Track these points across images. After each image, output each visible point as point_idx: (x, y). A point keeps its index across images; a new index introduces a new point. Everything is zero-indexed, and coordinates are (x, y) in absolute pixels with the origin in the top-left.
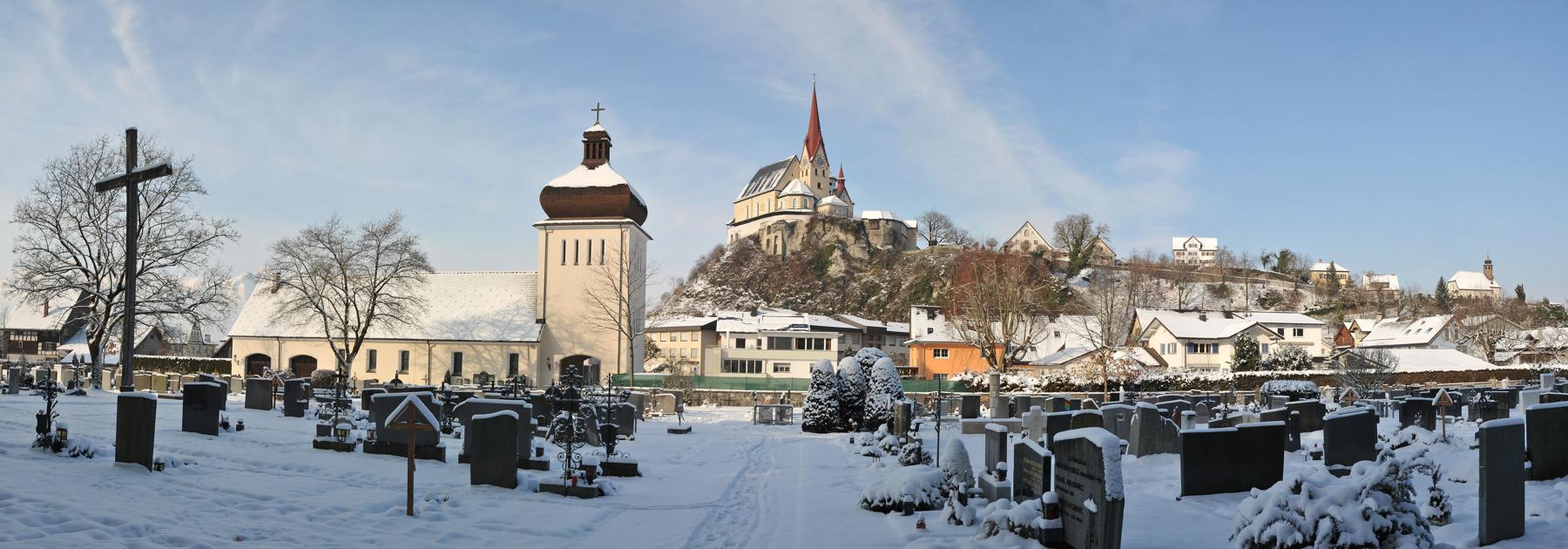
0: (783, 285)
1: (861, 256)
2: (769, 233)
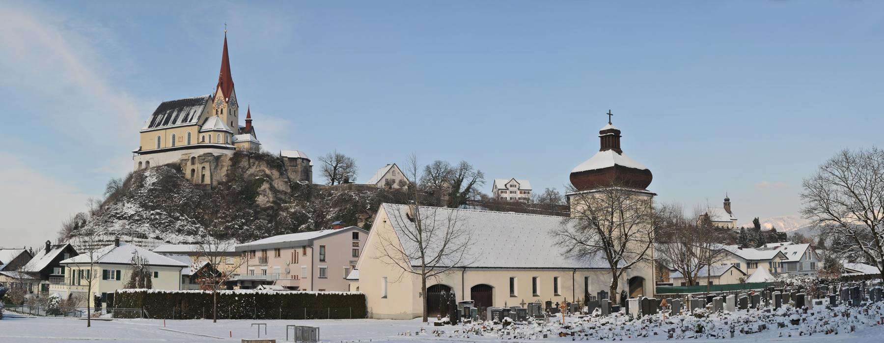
0: (217, 212)
1: (284, 189)
2: (193, 163)
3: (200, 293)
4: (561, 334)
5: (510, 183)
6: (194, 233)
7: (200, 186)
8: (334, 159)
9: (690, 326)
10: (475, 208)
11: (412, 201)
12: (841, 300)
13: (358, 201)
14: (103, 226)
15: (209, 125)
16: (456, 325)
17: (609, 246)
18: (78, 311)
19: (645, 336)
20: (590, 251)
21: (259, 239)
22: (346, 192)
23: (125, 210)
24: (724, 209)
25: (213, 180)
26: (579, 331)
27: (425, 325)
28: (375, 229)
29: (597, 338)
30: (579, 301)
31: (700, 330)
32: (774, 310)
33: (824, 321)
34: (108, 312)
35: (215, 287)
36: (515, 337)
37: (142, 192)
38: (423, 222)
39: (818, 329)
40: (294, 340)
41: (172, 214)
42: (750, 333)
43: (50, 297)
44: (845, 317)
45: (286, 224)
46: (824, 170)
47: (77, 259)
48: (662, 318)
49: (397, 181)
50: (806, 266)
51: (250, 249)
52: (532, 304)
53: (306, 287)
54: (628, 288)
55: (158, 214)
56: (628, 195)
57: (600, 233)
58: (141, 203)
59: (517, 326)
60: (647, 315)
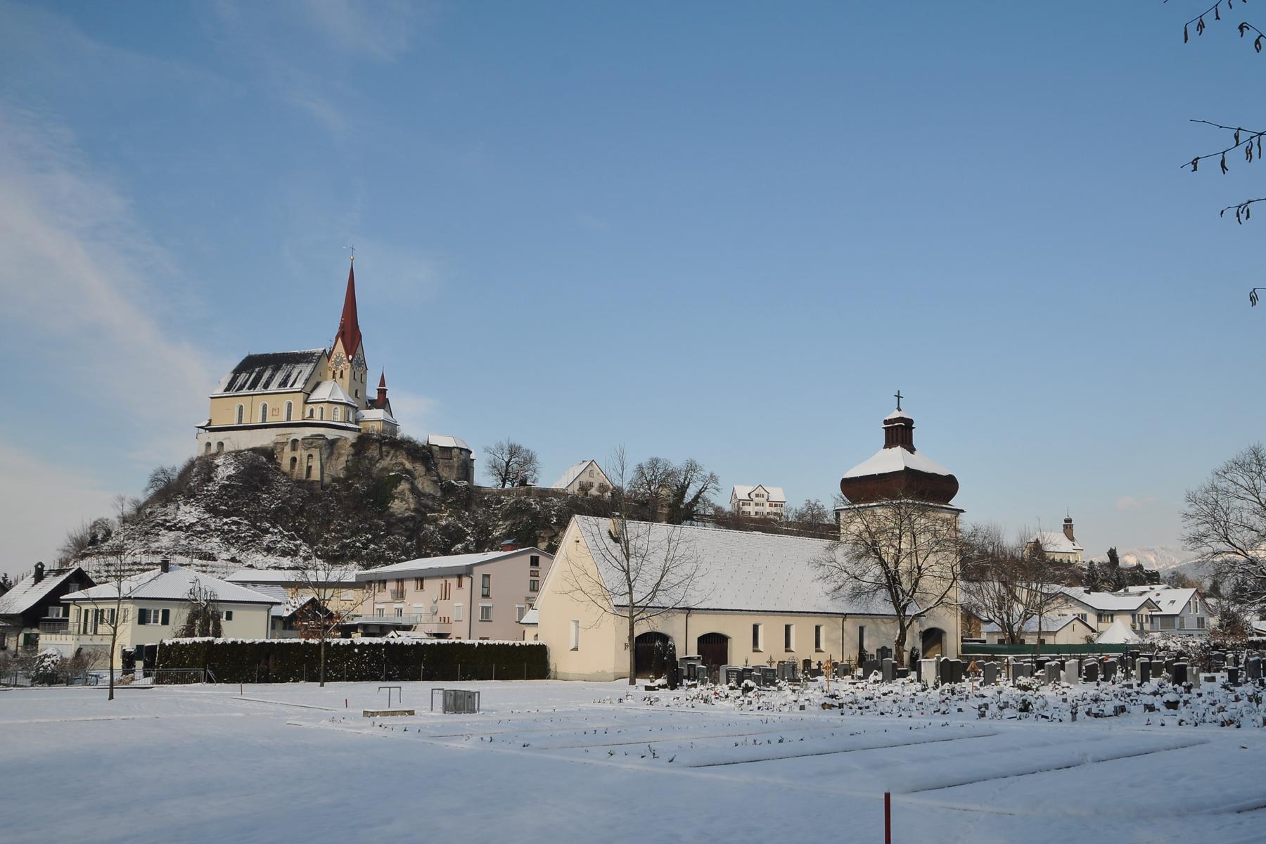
0: (329, 522)
1: (431, 492)
2: (294, 449)
3: (299, 643)
4: (824, 706)
5: (756, 492)
6: (294, 553)
7: (304, 484)
8: (506, 451)
9: (1011, 702)
10: (705, 526)
11: (618, 514)
12: (1246, 678)
13: (539, 512)
14: (141, 541)
15: (322, 393)
16: (676, 690)
17: (894, 583)
18: (92, 676)
19: (944, 713)
20: (866, 590)
21: (393, 563)
22: (523, 498)
23: (180, 516)
24: (1063, 534)
25: (325, 475)
26: (850, 702)
27: (632, 689)
28: (564, 552)
29: (877, 713)
30: (850, 661)
31: (1026, 707)
32: (1139, 685)
33: (1218, 705)
34: (146, 675)
35: (323, 634)
36: (759, 708)
37: (210, 488)
38: (632, 543)
39: (1209, 717)
40: (442, 710)
41: (258, 524)
42: (1101, 717)
43: (39, 655)
44: (1254, 704)
45: (434, 543)
46: (1220, 476)
47: (93, 592)
48: (970, 689)
49: (596, 485)
50: (1191, 623)
51: (378, 578)
52: (783, 662)
53: (460, 634)
54: (921, 643)
55: (234, 523)
56: (923, 510)
57: (882, 565)
58: (207, 505)
59: (762, 692)
60: (947, 684)
